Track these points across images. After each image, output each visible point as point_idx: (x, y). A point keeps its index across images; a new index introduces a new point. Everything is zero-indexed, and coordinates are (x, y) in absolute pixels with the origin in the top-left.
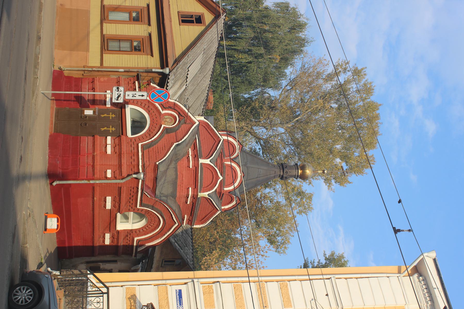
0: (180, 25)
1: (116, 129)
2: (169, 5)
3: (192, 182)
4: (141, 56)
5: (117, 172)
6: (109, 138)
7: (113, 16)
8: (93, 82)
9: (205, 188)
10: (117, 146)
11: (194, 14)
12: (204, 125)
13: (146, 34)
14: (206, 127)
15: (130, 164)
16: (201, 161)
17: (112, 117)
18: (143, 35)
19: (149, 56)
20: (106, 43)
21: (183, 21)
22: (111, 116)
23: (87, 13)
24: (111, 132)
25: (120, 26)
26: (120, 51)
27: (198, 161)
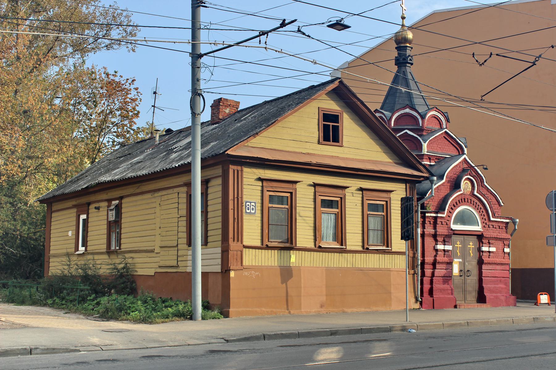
1: (472, 241)
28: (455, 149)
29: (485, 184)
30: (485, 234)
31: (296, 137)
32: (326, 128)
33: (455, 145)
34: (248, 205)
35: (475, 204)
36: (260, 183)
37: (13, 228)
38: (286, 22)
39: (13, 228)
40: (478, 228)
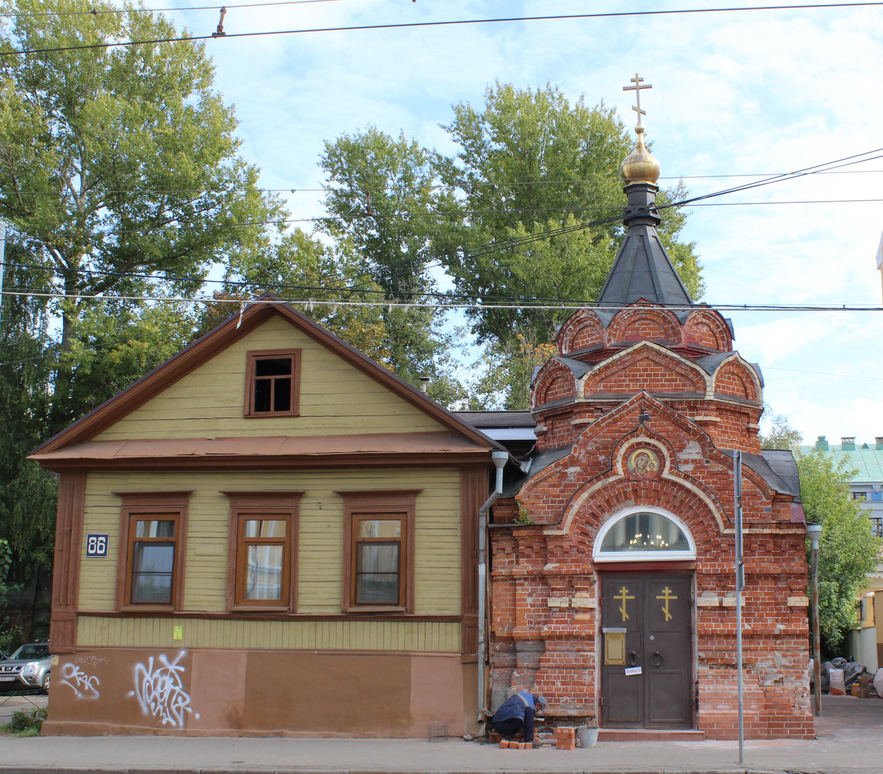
0: (298, 416)
2: (218, 439)
4: (417, 520)
7: (264, 586)
17: (627, 594)
19: (303, 501)
22: (624, 595)
23: (255, 656)
24: (632, 597)
25: (305, 570)
27: (710, 402)
31: (209, 411)
34: (93, 541)
38: (636, 106)
40: (689, 554)
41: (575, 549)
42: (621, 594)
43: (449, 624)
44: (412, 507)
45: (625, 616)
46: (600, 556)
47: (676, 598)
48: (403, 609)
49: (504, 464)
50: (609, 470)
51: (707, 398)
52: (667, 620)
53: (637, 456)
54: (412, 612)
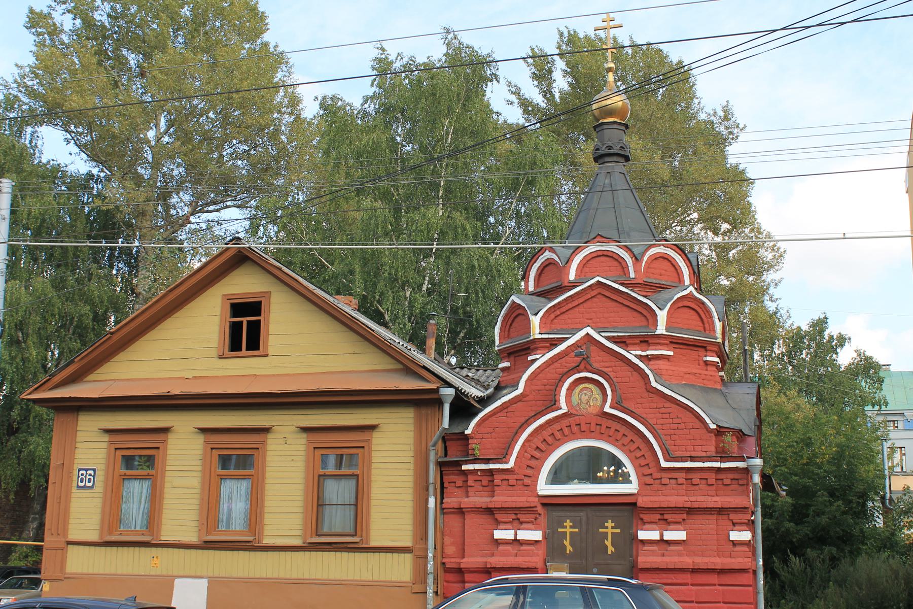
0: (267, 355)
1: (610, 517)
3: (693, 354)
5: (735, 517)
6: (643, 535)
8: (460, 571)
9: (707, 325)
10: (664, 516)
11: (229, 319)
12: (553, 316)
13: (199, 441)
14: (558, 312)
15: (714, 487)
16: (661, 329)
18: (303, 447)
19: (375, 434)
20: (328, 536)
21: (254, 343)
22: (568, 527)
26: (356, 505)
28: (635, 314)
29: (654, 384)
30: (641, 502)
32: (235, 329)
33: (632, 305)
35: (575, 429)
36: (106, 438)
37: (834, 468)
39: (834, 468)
40: (631, 488)
41: (520, 482)
42: (566, 527)
43: (402, 555)
44: (369, 441)
45: (569, 549)
46: (545, 488)
47: (618, 531)
48: (251, 539)
49: (450, 400)
50: (553, 404)
51: (658, 332)
52: (609, 552)
53: (581, 391)
54: (367, 543)
